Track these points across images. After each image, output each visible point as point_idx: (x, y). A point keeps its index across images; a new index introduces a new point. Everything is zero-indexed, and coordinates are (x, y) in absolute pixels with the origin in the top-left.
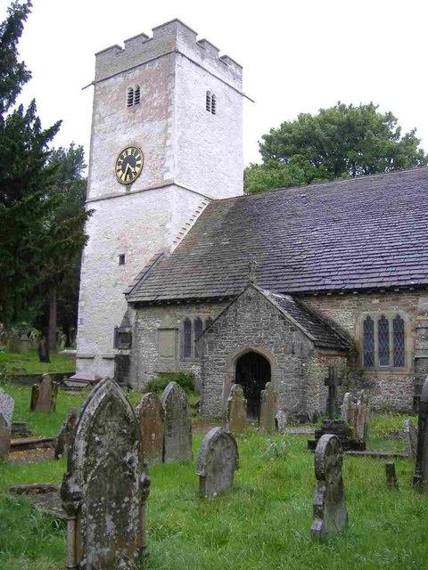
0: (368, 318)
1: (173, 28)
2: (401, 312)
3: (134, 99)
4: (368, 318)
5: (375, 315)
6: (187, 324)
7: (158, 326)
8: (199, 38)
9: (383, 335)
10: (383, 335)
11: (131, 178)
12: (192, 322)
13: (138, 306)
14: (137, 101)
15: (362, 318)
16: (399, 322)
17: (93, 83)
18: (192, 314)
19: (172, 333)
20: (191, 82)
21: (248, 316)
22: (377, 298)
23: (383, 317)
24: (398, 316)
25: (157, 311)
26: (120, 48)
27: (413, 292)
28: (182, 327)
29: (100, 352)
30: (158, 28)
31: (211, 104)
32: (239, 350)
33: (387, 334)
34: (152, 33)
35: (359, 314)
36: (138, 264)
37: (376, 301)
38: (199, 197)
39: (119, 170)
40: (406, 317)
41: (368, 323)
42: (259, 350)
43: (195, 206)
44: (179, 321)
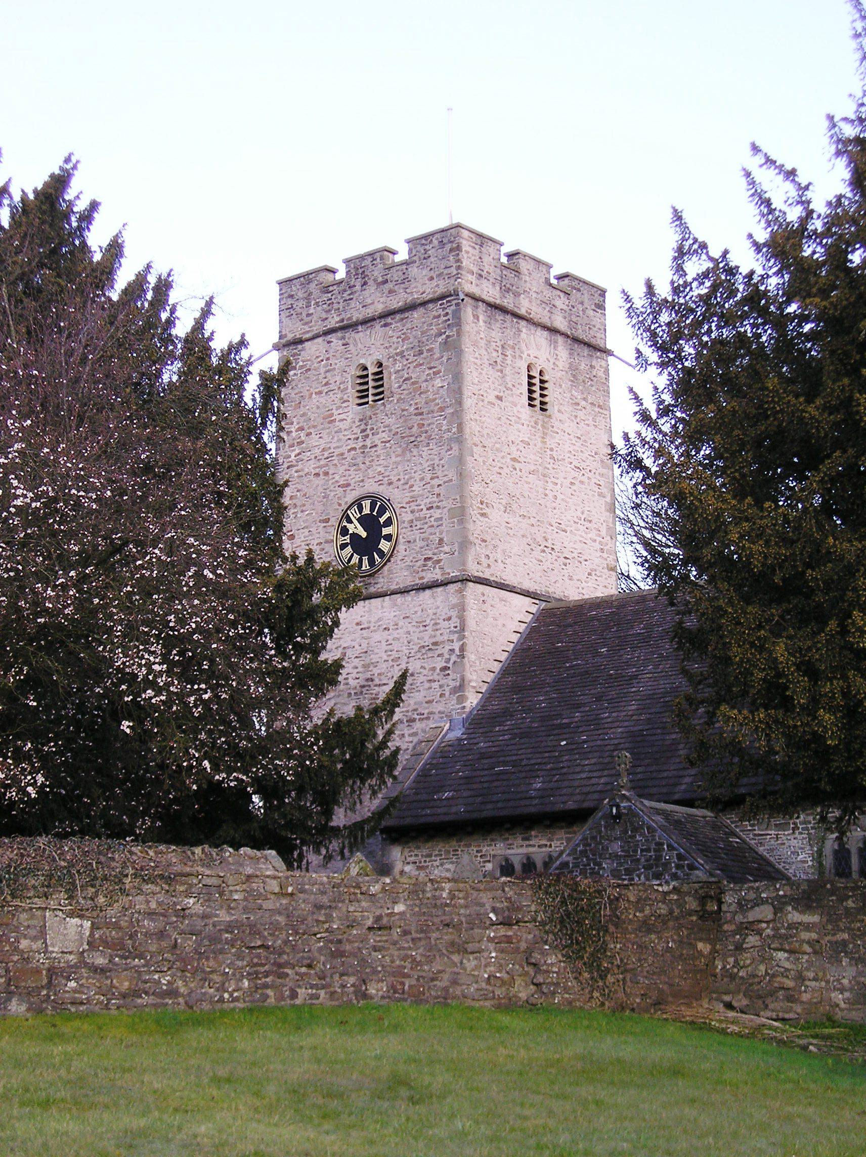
1: (443, 243)
3: (371, 386)
11: (372, 562)
25: (441, 846)
31: (537, 392)
39: (343, 546)
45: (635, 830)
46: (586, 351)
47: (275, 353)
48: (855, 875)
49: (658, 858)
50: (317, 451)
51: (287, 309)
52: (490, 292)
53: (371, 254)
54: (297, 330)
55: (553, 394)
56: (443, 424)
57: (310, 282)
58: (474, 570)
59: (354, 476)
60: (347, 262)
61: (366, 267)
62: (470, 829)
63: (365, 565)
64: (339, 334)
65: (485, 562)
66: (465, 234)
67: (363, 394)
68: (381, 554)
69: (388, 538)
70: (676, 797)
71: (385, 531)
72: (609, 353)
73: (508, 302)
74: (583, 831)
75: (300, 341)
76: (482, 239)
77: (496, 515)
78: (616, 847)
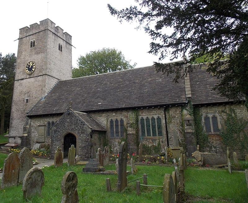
0: (112, 120)
1: (46, 22)
2: (122, 117)
3: (33, 44)
4: (112, 120)
5: (114, 119)
6: (49, 123)
7: (39, 125)
8: (56, 26)
9: (117, 126)
10: (117, 126)
11: (31, 72)
12: (150, 118)
13: (31, 117)
14: (34, 46)
15: (109, 120)
16: (122, 121)
17: (18, 39)
18: (51, 120)
19: (43, 128)
20: (52, 43)
21: (68, 120)
22: (114, 113)
23: (117, 119)
24: (122, 119)
25: (38, 119)
26: (28, 28)
27: (154, 108)
28: (47, 125)
29: (18, 135)
30: (41, 21)
31: (60, 48)
32: (65, 133)
33: (118, 126)
34: (39, 23)
35: (108, 119)
36: (31, 105)
37: (114, 114)
38: (55, 79)
39: (27, 70)
40: (124, 119)
41: (112, 121)
42: (72, 132)
43: (52, 83)
44: (46, 123)
45: (72, 117)
46: (68, 44)
47: (18, 40)
48: (152, 136)
49: (77, 123)
50: (24, 55)
51: (20, 33)
52: (54, 31)
53: (34, 24)
54: (21, 36)
55: (63, 49)
56: (43, 50)
57: (24, 29)
58: (48, 73)
59: (29, 59)
60: (30, 25)
61: (34, 26)
62: (200, 106)
63: (30, 73)
64: (28, 37)
65: (50, 72)
66: (49, 20)
67: (31, 46)
68: (33, 71)
69: (34, 68)
70: (81, 111)
71: (33, 67)
72: (72, 46)
73: (56, 33)
74: (61, 117)
75: (22, 38)
76: (52, 22)
77: (52, 65)
78: (68, 120)
